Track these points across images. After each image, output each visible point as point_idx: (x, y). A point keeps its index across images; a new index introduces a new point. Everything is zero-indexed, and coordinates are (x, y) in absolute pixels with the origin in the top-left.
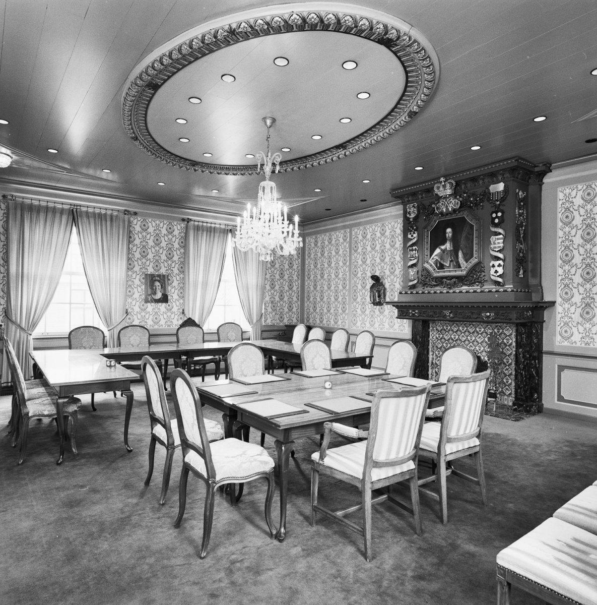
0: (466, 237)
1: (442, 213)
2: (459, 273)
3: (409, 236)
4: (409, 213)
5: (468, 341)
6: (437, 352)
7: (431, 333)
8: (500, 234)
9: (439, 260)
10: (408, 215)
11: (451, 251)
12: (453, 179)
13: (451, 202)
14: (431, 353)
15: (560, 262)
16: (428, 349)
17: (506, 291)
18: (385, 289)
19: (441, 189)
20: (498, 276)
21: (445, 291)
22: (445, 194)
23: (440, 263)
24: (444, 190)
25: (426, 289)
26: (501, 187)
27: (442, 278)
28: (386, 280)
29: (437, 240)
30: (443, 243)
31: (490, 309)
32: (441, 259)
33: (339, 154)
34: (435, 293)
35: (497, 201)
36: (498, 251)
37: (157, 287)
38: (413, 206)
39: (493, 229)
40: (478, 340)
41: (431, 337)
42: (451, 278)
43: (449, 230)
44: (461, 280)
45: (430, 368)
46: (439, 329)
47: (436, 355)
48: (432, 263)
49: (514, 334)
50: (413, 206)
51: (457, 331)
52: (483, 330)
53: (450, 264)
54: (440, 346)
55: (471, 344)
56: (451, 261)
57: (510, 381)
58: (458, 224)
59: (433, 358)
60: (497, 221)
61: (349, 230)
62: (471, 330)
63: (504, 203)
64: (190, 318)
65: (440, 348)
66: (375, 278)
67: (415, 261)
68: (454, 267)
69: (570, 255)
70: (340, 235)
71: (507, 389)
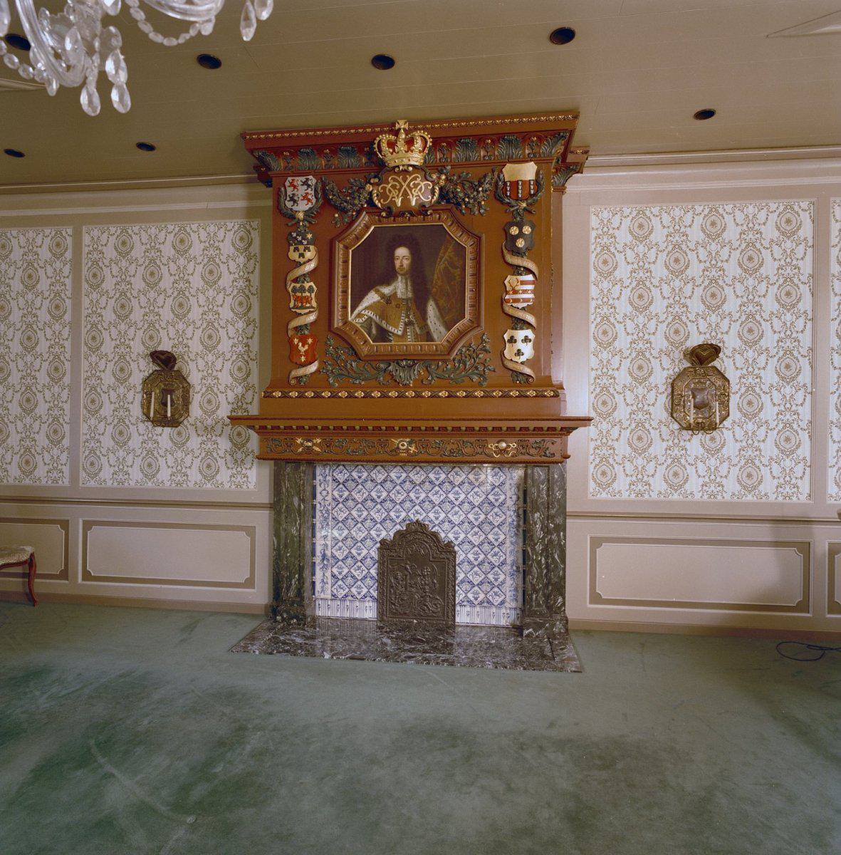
1: (389, 210)
3: (294, 256)
4: (292, 199)
5: (411, 501)
7: (319, 489)
9: (376, 318)
10: (289, 204)
11: (407, 300)
12: (425, 129)
13: (416, 186)
15: (593, 344)
18: (187, 388)
19: (401, 146)
20: (522, 363)
22: (405, 161)
28: (192, 366)
38: (305, 183)
40: (434, 498)
41: (319, 497)
43: (402, 252)
45: (318, 568)
46: (341, 478)
50: (305, 183)
51: (385, 481)
53: (405, 332)
54: (342, 516)
55: (417, 507)
56: (406, 324)
57: (502, 577)
59: (326, 545)
61: (70, 231)
66: (164, 360)
69: (610, 334)
70: (43, 240)
71: (496, 594)
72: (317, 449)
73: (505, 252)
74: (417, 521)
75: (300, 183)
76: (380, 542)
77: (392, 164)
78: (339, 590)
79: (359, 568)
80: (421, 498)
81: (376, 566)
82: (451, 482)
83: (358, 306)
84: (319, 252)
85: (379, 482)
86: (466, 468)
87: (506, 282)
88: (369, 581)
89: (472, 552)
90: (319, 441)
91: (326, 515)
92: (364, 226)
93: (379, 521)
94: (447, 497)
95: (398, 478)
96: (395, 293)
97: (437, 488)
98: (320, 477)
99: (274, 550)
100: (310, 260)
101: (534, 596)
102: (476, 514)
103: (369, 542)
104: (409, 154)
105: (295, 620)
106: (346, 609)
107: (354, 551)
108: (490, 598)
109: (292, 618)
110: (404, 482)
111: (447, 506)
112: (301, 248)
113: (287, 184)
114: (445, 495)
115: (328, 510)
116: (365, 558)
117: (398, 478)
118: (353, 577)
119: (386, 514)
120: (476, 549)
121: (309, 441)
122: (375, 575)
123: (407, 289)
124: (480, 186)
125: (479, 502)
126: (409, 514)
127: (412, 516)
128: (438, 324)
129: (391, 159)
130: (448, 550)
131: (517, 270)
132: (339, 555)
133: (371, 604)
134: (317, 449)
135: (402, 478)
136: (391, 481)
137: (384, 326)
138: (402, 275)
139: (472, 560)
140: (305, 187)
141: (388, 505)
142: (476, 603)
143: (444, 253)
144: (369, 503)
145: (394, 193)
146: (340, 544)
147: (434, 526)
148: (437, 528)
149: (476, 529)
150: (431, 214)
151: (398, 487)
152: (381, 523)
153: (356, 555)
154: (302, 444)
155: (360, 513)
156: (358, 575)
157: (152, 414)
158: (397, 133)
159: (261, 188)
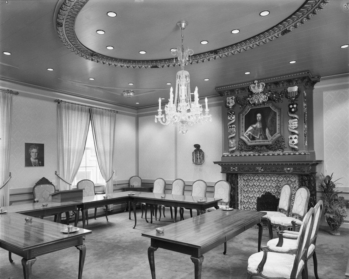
0: (271, 120)
1: (254, 104)
2: (266, 143)
6: (244, 194)
7: (239, 182)
8: (295, 118)
9: (252, 134)
10: (228, 105)
11: (260, 128)
12: (263, 82)
13: (261, 97)
14: (239, 195)
16: (238, 193)
17: (300, 154)
19: (256, 87)
20: (294, 145)
21: (257, 155)
22: (258, 91)
23: (252, 136)
24: (258, 89)
25: (242, 153)
26: (296, 89)
27: (255, 146)
29: (250, 120)
30: (255, 122)
31: (290, 166)
32: (253, 134)
33: (210, 57)
34: (268, 155)
35: (293, 97)
36: (294, 129)
37: (35, 154)
38: (232, 98)
39: (291, 115)
41: (239, 184)
42: (261, 146)
44: (269, 147)
45: (239, 205)
46: (245, 179)
47: (244, 196)
48: (246, 136)
49: (297, 180)
50: (232, 98)
51: (258, 180)
52: (276, 179)
53: (260, 137)
55: (268, 188)
56: (260, 135)
58: (265, 111)
59: (242, 198)
60: (293, 110)
62: (268, 179)
63: (297, 99)
64: (44, 178)
65: (246, 192)
67: (234, 135)
68: (263, 139)
72: (236, 170)
73: (289, 113)
76: (257, 198)
77: (254, 92)
79: (251, 205)
80: (269, 185)
81: (256, 205)
82: (278, 180)
84: (236, 117)
87: (289, 122)
90: (237, 168)
92: (248, 109)
94: (277, 185)
95: (262, 179)
96: (257, 127)
97: (274, 182)
98: (240, 179)
100: (233, 119)
104: (259, 89)
107: (249, 200)
110: (264, 180)
112: (231, 116)
113: (227, 99)
115: (242, 188)
116: (253, 202)
118: (249, 208)
121: (234, 168)
122: (256, 208)
123: (260, 125)
124: (280, 95)
129: (254, 91)
131: (293, 118)
132: (246, 201)
134: (236, 170)
137: (254, 136)
140: (232, 100)
141: (259, 187)
144: (254, 186)
145: (256, 100)
146: (246, 198)
147: (274, 194)
148: (274, 194)
150: (266, 104)
152: (257, 192)
153: (250, 201)
154: (232, 169)
157: (195, 161)
158: (255, 84)
159: (221, 97)
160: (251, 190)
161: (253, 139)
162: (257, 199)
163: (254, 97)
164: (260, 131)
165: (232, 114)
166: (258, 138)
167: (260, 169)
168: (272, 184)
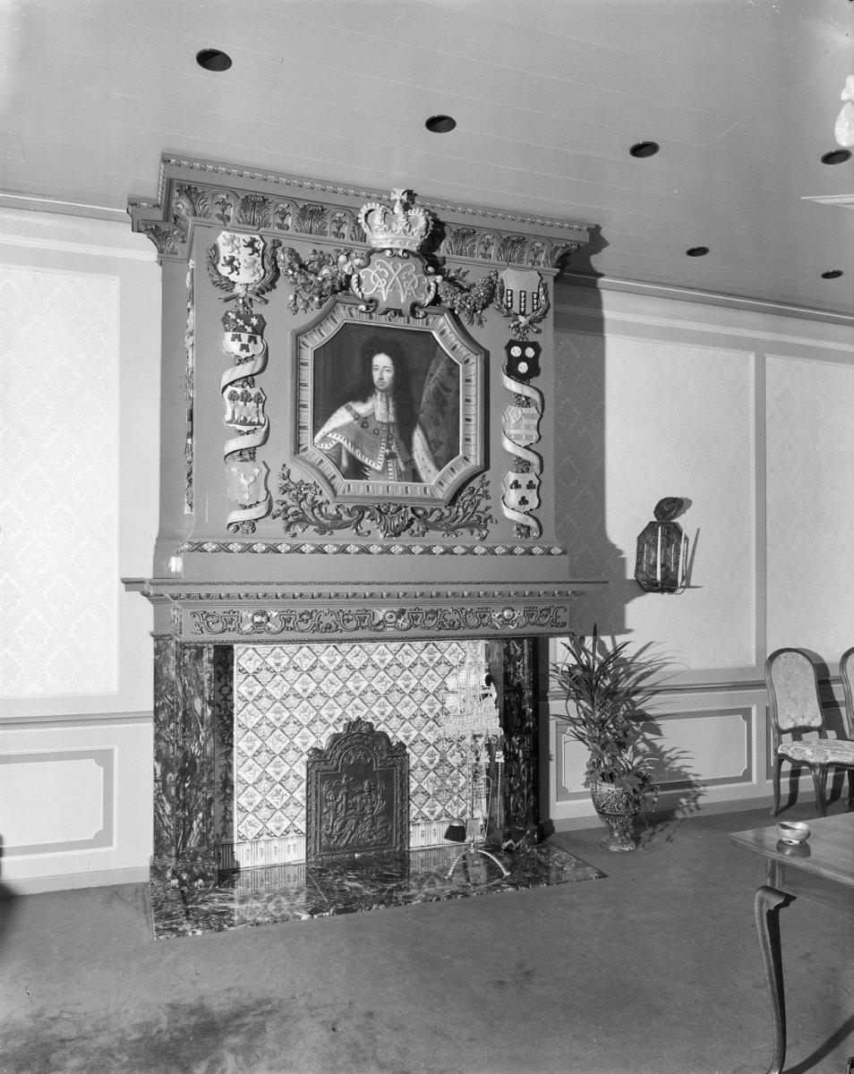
4: (230, 262)
10: (225, 271)
11: (388, 424)
23: (352, 458)
29: (339, 378)
30: (365, 390)
32: (355, 445)
38: (251, 244)
40: (377, 687)
43: (382, 362)
50: (251, 244)
51: (313, 668)
53: (385, 466)
55: (357, 701)
60: (523, 367)
68: (401, 476)
74: (359, 719)
75: (243, 243)
78: (249, 828)
79: (278, 793)
83: (322, 426)
85: (305, 669)
86: (419, 645)
88: (292, 810)
89: (426, 753)
91: (228, 722)
93: (305, 724)
96: (374, 414)
99: (156, 781)
101: (512, 799)
102: (432, 704)
103: (291, 755)
105: (201, 881)
106: (259, 854)
108: (449, 810)
109: (196, 880)
111: (395, 697)
114: (392, 682)
117: (331, 662)
119: (315, 712)
120: (431, 748)
122: (300, 799)
123: (388, 409)
125: (434, 688)
126: (347, 711)
127: (350, 714)
128: (427, 459)
130: (398, 752)
133: (295, 841)
135: (336, 663)
136: (322, 668)
137: (359, 457)
138: (382, 391)
139: (427, 763)
141: (318, 700)
142: (432, 818)
143: (435, 369)
144: (292, 701)
147: (379, 724)
149: (431, 723)
151: (331, 676)
152: (308, 726)
155: (278, 716)
156: (277, 803)
160: (331, 716)
161: (357, 470)
162: (306, 758)
163: (374, 268)
164: (388, 439)
165: (249, 329)
166: (379, 468)
167: (391, 617)
168: (446, 655)
